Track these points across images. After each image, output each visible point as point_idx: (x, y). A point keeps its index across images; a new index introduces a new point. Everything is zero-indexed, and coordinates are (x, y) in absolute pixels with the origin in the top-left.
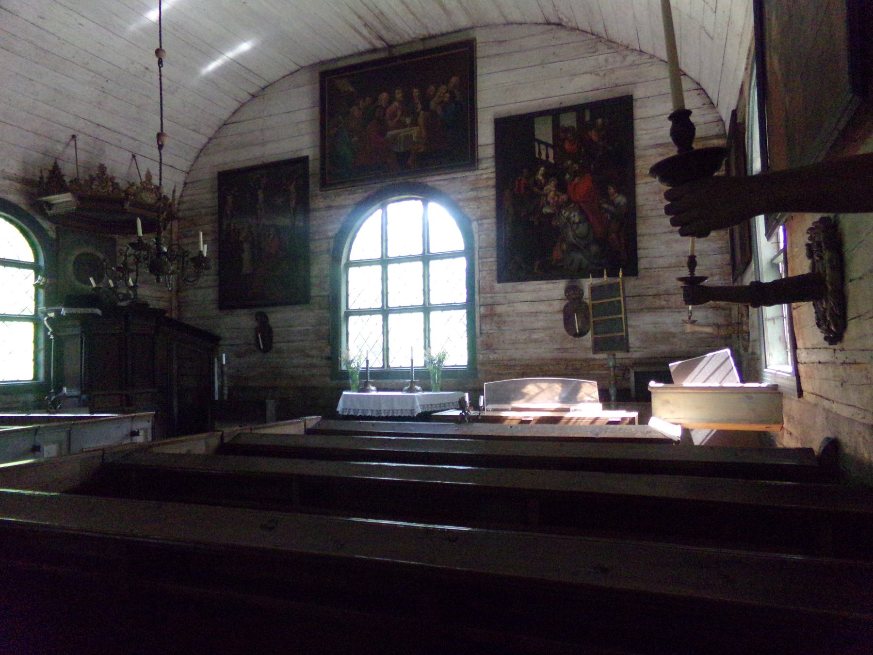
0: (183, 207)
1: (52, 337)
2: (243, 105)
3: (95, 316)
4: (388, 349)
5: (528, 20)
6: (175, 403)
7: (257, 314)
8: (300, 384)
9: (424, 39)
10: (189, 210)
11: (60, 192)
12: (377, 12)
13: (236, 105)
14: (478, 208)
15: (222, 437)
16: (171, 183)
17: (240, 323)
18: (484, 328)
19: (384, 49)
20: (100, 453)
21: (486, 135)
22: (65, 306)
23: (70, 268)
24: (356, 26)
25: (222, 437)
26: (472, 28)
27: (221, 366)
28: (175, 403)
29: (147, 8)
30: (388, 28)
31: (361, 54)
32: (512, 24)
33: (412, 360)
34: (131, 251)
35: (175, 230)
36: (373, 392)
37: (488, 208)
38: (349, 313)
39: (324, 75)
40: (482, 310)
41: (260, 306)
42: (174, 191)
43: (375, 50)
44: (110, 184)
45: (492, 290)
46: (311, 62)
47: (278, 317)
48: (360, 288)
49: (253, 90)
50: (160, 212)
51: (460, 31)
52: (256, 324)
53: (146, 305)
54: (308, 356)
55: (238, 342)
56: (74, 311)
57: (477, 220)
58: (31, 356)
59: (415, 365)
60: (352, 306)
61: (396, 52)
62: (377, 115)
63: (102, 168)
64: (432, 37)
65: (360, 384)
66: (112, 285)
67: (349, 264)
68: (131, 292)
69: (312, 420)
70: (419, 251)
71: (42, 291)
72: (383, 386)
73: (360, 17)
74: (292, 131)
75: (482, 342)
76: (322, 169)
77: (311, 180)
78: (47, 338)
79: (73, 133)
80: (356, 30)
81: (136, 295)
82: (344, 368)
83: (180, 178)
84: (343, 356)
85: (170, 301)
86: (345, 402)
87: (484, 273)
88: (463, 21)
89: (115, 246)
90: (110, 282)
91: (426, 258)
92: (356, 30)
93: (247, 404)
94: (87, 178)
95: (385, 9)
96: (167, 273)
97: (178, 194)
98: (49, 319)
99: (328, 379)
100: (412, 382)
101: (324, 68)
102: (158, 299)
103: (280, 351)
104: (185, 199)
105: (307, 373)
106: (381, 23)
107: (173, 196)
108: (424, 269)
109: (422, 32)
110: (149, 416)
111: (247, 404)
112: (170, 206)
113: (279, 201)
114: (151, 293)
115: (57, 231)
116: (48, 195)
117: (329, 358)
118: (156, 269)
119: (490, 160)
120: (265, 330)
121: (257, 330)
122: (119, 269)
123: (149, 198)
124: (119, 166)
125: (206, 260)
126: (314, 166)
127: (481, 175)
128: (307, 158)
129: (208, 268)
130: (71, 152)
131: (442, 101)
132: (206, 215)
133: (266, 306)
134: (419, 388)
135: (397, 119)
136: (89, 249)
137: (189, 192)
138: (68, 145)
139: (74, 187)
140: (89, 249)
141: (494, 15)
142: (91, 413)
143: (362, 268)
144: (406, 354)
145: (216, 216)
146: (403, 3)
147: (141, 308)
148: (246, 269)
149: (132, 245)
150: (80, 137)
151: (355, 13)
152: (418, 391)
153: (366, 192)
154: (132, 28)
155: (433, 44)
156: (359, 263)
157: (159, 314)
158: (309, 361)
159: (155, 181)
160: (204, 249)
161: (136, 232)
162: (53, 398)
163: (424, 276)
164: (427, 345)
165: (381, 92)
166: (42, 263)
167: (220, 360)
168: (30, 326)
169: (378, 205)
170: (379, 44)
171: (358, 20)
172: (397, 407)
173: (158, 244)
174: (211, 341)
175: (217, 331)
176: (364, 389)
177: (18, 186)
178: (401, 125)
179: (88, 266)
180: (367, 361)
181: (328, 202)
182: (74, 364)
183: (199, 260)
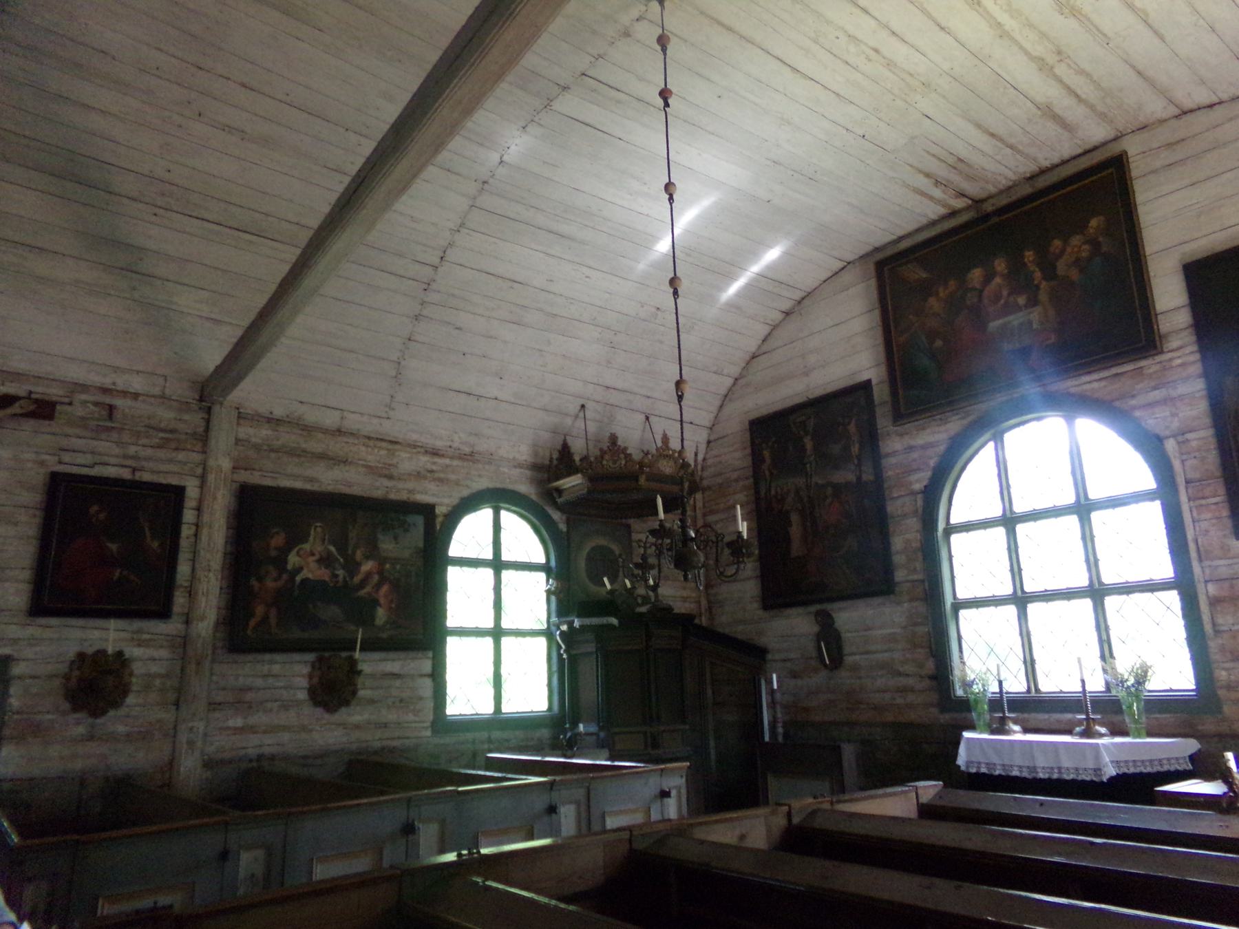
0: (706, 474)
1: (565, 656)
2: (775, 327)
3: (610, 627)
4: (1033, 662)
5: (1225, 97)
6: (712, 743)
7: (817, 613)
8: (889, 717)
9: (1032, 178)
10: (715, 476)
11: (569, 475)
12: (951, 160)
13: (767, 329)
14: (1173, 415)
15: (789, 815)
16: (694, 443)
17: (792, 629)
18: (1220, 620)
19: (968, 208)
20: (626, 835)
21: (1169, 296)
22: (579, 616)
23: (582, 564)
24: (923, 188)
25: (789, 815)
26: (1116, 139)
27: (772, 692)
28: (712, 743)
29: (656, 239)
30: (969, 178)
31: (933, 223)
32: (1191, 111)
33: (1083, 682)
34: (652, 539)
35: (699, 504)
36: (1017, 735)
37: (1194, 413)
38: (959, 605)
39: (880, 266)
40: (1212, 589)
41: (821, 601)
42: (696, 454)
43: (953, 214)
44: (622, 456)
45: (1226, 552)
46: (862, 252)
47: (848, 617)
48: (973, 564)
49: (786, 306)
50: (682, 485)
51: (1095, 148)
52: (816, 629)
53: (669, 609)
54: (900, 674)
55: (792, 656)
56: (588, 621)
57: (1174, 436)
58: (545, 681)
59: (1088, 688)
60: (962, 594)
61: (989, 207)
62: (968, 303)
63: (613, 439)
64: (1043, 172)
65: (992, 718)
66: (629, 585)
67: (950, 530)
68: (651, 593)
69: (929, 789)
70: (1069, 498)
71: (553, 598)
72: (1032, 725)
73: (927, 175)
74: (844, 349)
75: (1223, 649)
76: (894, 393)
77: (879, 411)
78: (560, 655)
79: (582, 402)
80: (923, 194)
81: (657, 596)
82: (960, 692)
83: (702, 436)
84: (957, 672)
85: (699, 602)
86: (968, 749)
87: (1204, 525)
88: (1096, 133)
89: (630, 534)
90: (627, 582)
91: (1083, 508)
92: (923, 194)
93: (811, 751)
94: (598, 453)
95: (963, 152)
96: (694, 568)
97: (700, 457)
98: (562, 633)
99: (934, 711)
100: (1088, 719)
101: (880, 256)
102: (684, 599)
103: (855, 668)
104: (710, 462)
105: (899, 701)
106: (961, 173)
107: (696, 461)
108: (1083, 527)
109: (1029, 168)
110: (680, 768)
111: (811, 751)
112: (692, 474)
113: (836, 449)
114: (675, 593)
115: (568, 522)
116: (558, 479)
117: (933, 678)
118: (683, 562)
119: (1186, 333)
120: (829, 636)
121: (818, 638)
122: (637, 565)
123: (667, 468)
124: (633, 435)
125: (746, 544)
126: (881, 393)
127: (1171, 360)
128: (869, 381)
129: (749, 555)
130: (580, 424)
131: (1078, 260)
132: (736, 480)
133: (832, 600)
134: (1103, 730)
135: (1002, 302)
136: (601, 541)
137: (714, 452)
138: (577, 417)
139: (585, 466)
140: (601, 541)
141: (1155, 107)
142: (612, 758)
143: (972, 534)
144: (1068, 669)
145: (751, 480)
146: (1131, 7)
147: (663, 615)
148: (797, 548)
149: (653, 532)
150: (589, 405)
151: (920, 171)
152: (1102, 735)
153: (963, 418)
154: (641, 267)
155: (1042, 183)
156: (967, 527)
157: (686, 621)
158: (903, 681)
159: (675, 444)
160: (743, 527)
161: (656, 514)
162: (569, 734)
163: (1084, 538)
164: (1106, 654)
165: (969, 270)
166: (553, 563)
167: (770, 682)
168: (542, 642)
169: (987, 435)
170: (959, 203)
171: (926, 180)
172: (1066, 763)
173: (684, 527)
174: (754, 655)
175: (763, 641)
176: (1001, 728)
177: (528, 473)
178: (1009, 309)
179: (604, 563)
180: (1000, 683)
181: (908, 441)
182: (590, 693)
183: (737, 547)
